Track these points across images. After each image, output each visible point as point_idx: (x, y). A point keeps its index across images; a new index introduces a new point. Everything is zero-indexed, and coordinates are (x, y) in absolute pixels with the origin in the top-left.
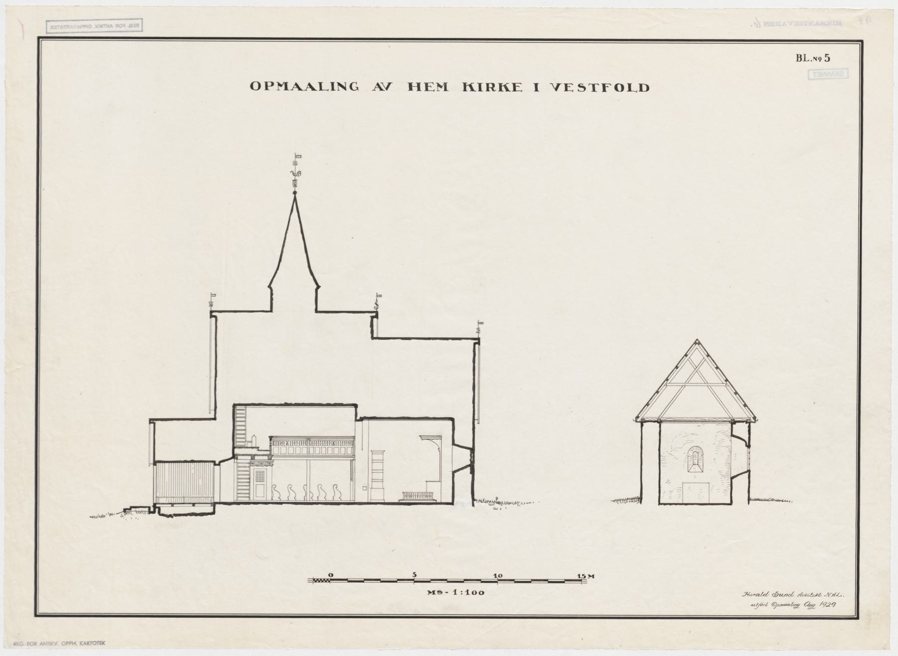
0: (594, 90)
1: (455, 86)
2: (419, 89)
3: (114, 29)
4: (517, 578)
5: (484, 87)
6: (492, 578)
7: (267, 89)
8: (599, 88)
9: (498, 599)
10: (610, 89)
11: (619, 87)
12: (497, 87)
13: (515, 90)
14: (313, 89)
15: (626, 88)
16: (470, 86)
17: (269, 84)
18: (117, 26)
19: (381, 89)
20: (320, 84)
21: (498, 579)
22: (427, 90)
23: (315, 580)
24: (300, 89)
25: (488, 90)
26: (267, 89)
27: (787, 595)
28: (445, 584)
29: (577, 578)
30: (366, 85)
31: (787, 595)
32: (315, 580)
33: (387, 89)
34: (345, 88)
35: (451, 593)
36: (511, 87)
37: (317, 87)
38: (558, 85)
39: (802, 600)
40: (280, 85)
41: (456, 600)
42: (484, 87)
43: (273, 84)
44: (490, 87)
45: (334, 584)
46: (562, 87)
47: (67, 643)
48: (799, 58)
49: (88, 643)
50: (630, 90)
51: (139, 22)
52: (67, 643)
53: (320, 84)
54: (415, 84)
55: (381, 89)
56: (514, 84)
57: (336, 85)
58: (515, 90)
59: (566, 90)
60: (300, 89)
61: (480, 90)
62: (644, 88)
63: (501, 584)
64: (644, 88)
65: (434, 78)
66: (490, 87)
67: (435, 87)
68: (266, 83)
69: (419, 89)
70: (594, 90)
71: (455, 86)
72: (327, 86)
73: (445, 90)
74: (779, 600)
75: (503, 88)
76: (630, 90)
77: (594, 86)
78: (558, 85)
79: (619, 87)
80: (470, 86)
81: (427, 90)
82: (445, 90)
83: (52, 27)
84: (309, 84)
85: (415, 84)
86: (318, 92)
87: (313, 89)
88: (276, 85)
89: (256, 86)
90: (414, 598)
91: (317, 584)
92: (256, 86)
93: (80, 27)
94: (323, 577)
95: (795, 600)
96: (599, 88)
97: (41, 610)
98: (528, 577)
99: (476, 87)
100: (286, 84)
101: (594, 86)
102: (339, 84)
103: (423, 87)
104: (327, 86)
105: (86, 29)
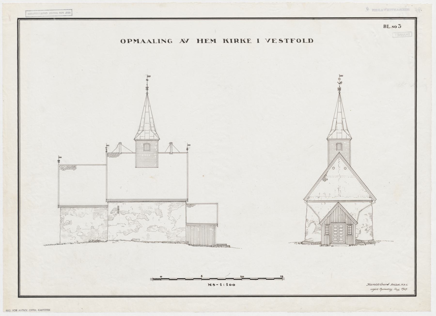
0: (287, 42)
1: (220, 41)
4: (265, 280)
6: (240, 277)
8: (289, 41)
9: (242, 288)
10: (295, 41)
12: (240, 41)
13: (248, 42)
14: (150, 42)
17: (130, 40)
18: (60, 13)
19: (184, 42)
20: (154, 40)
21: (242, 278)
24: (144, 42)
33: (187, 42)
34: (165, 42)
36: (246, 41)
37: (152, 41)
38: (269, 39)
41: (223, 288)
42: (233, 41)
43: (131, 40)
44: (236, 41)
46: (271, 41)
50: (304, 42)
51: (71, 11)
52: (42, 310)
53: (154, 40)
55: (184, 42)
56: (248, 39)
57: (161, 41)
58: (248, 42)
59: (273, 42)
60: (144, 42)
62: (311, 41)
63: (243, 280)
65: (210, 37)
66: (236, 41)
67: (210, 41)
70: (287, 42)
72: (156, 41)
74: (383, 287)
76: (304, 42)
77: (287, 40)
78: (269, 39)
83: (29, 14)
85: (200, 40)
87: (150, 42)
88: (133, 40)
89: (123, 41)
90: (201, 288)
92: (123, 41)
95: (389, 287)
96: (289, 41)
97: (413, 293)
99: (246, 41)
100: (138, 40)
101: (287, 40)
102: (162, 40)
103: (204, 41)
104: (156, 41)
105: (45, 15)
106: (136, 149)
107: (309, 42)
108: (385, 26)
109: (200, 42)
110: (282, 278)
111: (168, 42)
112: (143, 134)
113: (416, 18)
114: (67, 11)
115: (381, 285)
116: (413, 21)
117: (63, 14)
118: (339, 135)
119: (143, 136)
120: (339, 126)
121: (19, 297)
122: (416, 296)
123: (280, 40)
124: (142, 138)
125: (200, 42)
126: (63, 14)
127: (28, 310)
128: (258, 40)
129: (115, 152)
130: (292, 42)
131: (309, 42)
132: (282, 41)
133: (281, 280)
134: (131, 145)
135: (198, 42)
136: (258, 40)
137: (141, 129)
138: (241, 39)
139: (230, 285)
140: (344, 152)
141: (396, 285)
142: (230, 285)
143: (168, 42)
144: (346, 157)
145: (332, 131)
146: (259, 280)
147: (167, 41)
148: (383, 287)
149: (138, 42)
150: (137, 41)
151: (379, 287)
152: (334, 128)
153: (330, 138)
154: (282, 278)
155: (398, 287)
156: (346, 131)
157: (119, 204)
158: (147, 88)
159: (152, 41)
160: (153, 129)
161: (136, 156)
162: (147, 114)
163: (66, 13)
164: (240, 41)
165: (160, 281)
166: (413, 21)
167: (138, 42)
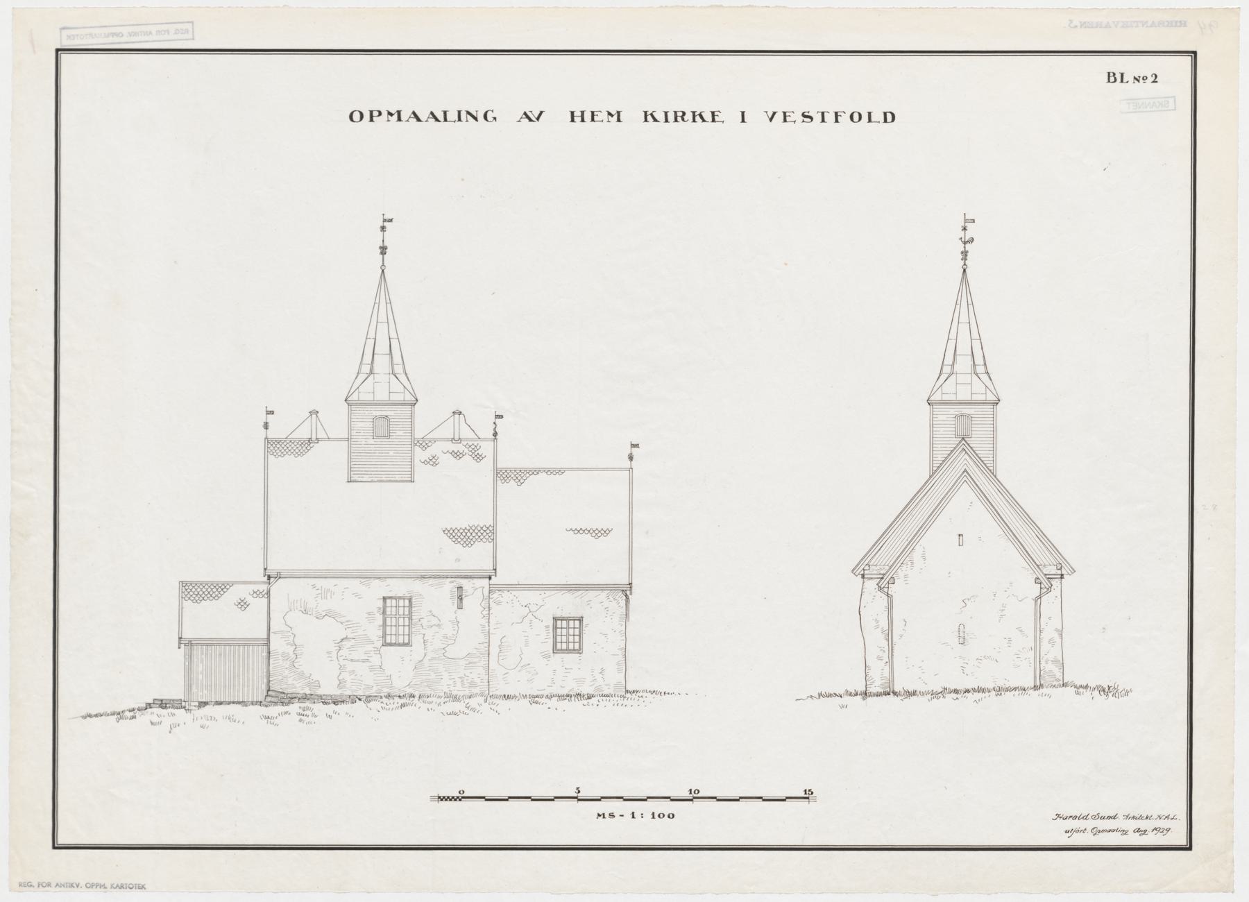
0: (823, 121)
1: (632, 115)
2: (583, 120)
3: (155, 38)
4: (760, 803)
5: (671, 117)
6: (686, 795)
7: (371, 120)
8: (830, 117)
9: (695, 823)
10: (844, 118)
11: (856, 117)
12: (689, 116)
13: (713, 120)
14: (437, 120)
15: (865, 117)
16: (701, 116)
17: (375, 114)
18: (158, 32)
19: (530, 120)
20: (445, 113)
21: (694, 796)
22: (593, 120)
23: (441, 799)
24: (419, 120)
25: (676, 120)
26: (371, 120)
27: (1109, 817)
28: (620, 803)
29: (803, 795)
30: (508, 113)
31: (1109, 817)
32: (441, 799)
33: (538, 119)
34: (476, 119)
35: (648, 816)
36: (708, 117)
37: (441, 117)
38: (774, 113)
39: (1131, 825)
40: (390, 114)
41: (644, 827)
42: (671, 117)
43: (380, 114)
44: (680, 117)
45: (464, 803)
46: (779, 116)
47: (92, 886)
48: (1111, 77)
49: (121, 887)
50: (870, 120)
51: (189, 26)
52: (92, 886)
53: (445, 113)
54: (577, 113)
55: (530, 120)
56: (713, 113)
57: (463, 115)
58: (713, 120)
59: (785, 120)
60: (419, 120)
61: (667, 121)
62: (889, 117)
63: (697, 803)
64: (889, 117)
65: (602, 107)
66: (680, 117)
67: (604, 116)
68: (371, 112)
69: (583, 120)
70: (823, 121)
71: (632, 115)
72: (452, 116)
73: (619, 120)
74: (1101, 824)
75: (649, 118)
76: (870, 120)
77: (823, 114)
78: (774, 113)
79: (856, 117)
80: (701, 116)
81: (593, 120)
82: (619, 120)
83: (69, 37)
84: (432, 113)
85: (577, 113)
86: (443, 124)
87: (437, 120)
88: (385, 114)
89: (356, 116)
90: (576, 824)
91: (444, 803)
92: (356, 116)
93: (107, 36)
94: (451, 795)
95: (1120, 823)
96: (830, 117)
97: (61, 840)
98: (736, 795)
99: (708, 117)
100: (399, 112)
101: (823, 114)
102: (468, 113)
103: (588, 116)
104: (452, 116)
105: (116, 39)
106: (350, 428)
107: (885, 121)
108: (1111, 77)
109: (578, 119)
110: (808, 796)
111: (485, 117)
112: (949, 387)
113: (1195, 53)
114: (179, 26)
115: (1094, 818)
116: (65, 57)
117: (166, 37)
118: (381, 387)
119: (950, 390)
120: (963, 364)
121: (54, 848)
122: (1190, 849)
123: (803, 115)
124: (946, 398)
125: (578, 119)
126: (166, 37)
127: (53, 885)
128: (743, 113)
129: (429, 436)
130: (837, 121)
131: (885, 121)
132: (811, 118)
133: (804, 803)
134: (335, 420)
135: (573, 120)
136: (743, 113)
137: (946, 372)
138: (694, 113)
139: (661, 816)
140: (978, 440)
141: (1141, 818)
142: (661, 816)
143: (485, 117)
144: (984, 453)
145: (943, 377)
146: (557, 802)
147: (481, 117)
148: (1101, 824)
149: (399, 119)
150: (615, 117)
151: (1090, 824)
152: (947, 370)
153: (354, 397)
154: (808, 796)
155: (1143, 824)
156: (985, 378)
157: (463, 582)
158: (383, 250)
159: (441, 117)
160: (980, 369)
161: (349, 447)
162: (964, 328)
163: (177, 31)
164: (689, 116)
165: (458, 802)
166: (65, 57)
167: (399, 119)
